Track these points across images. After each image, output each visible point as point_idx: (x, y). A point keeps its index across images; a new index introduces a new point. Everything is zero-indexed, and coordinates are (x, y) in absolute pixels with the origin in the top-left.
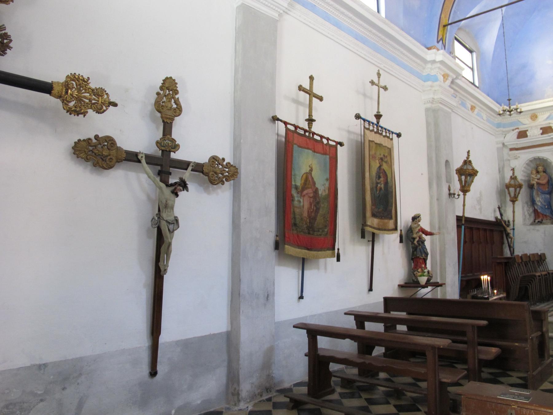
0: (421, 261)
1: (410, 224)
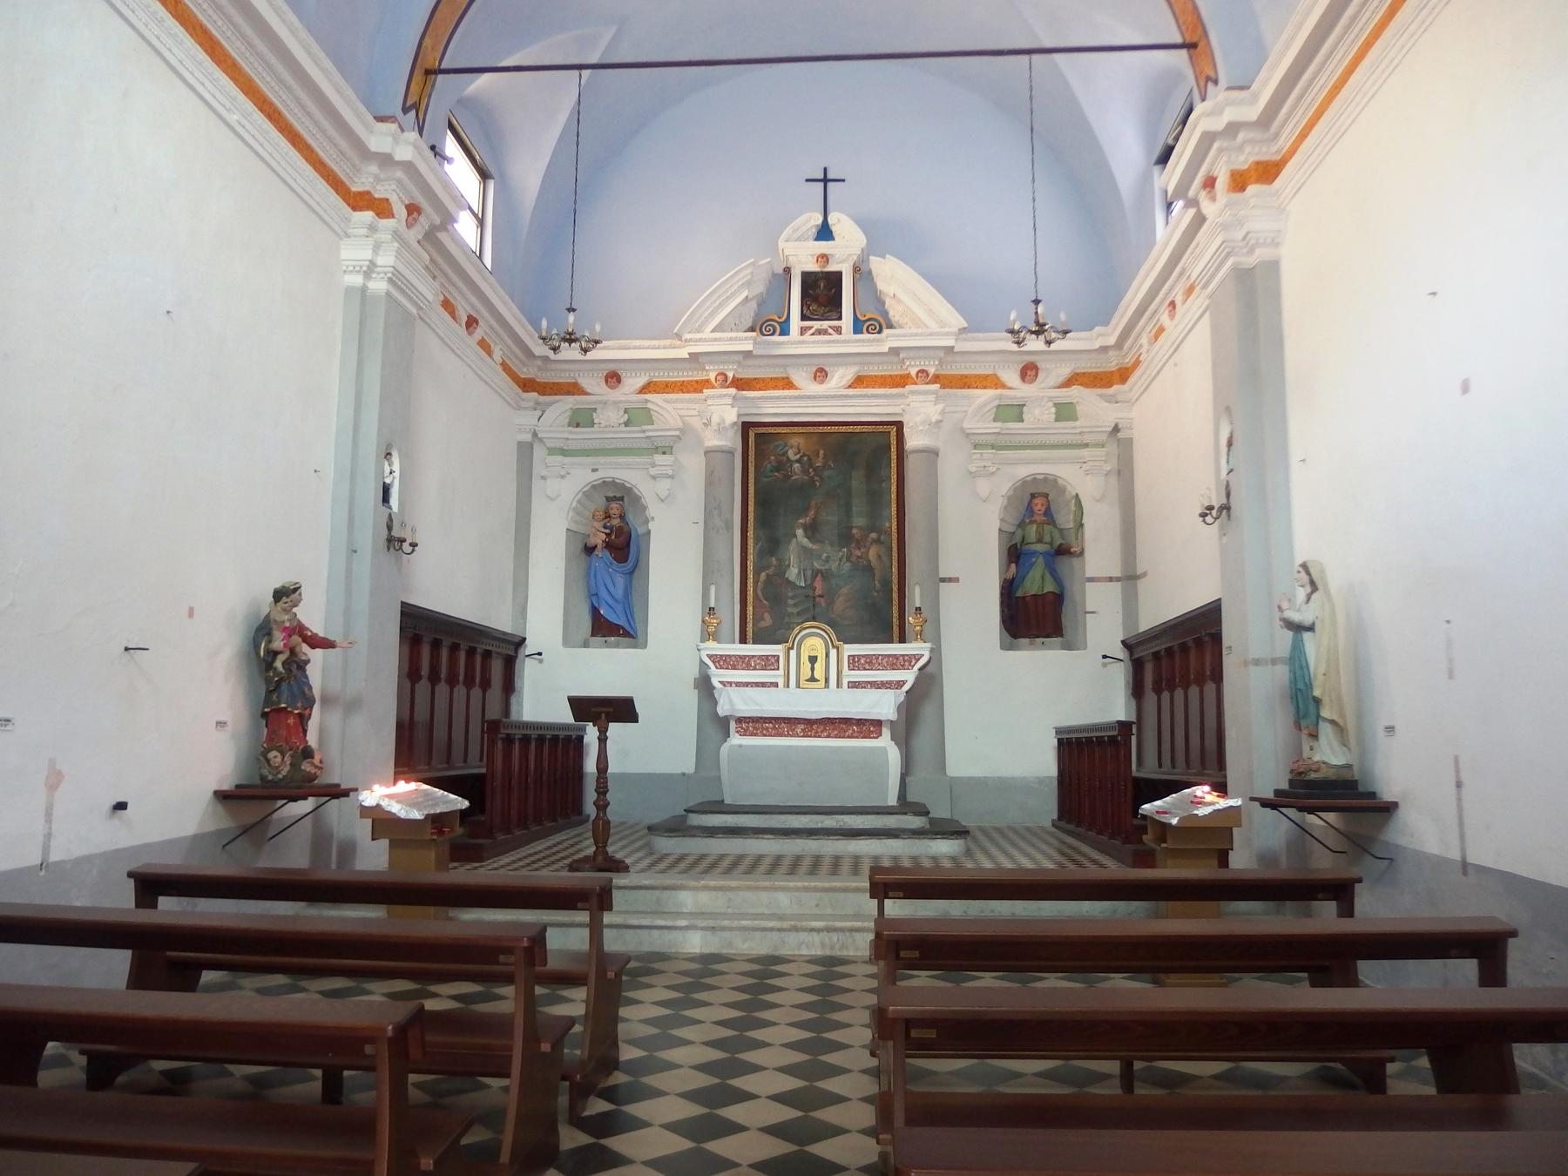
1: (265, 610)
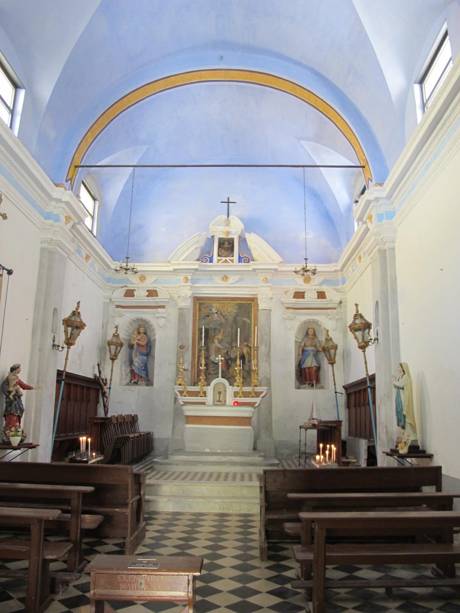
1: (7, 375)
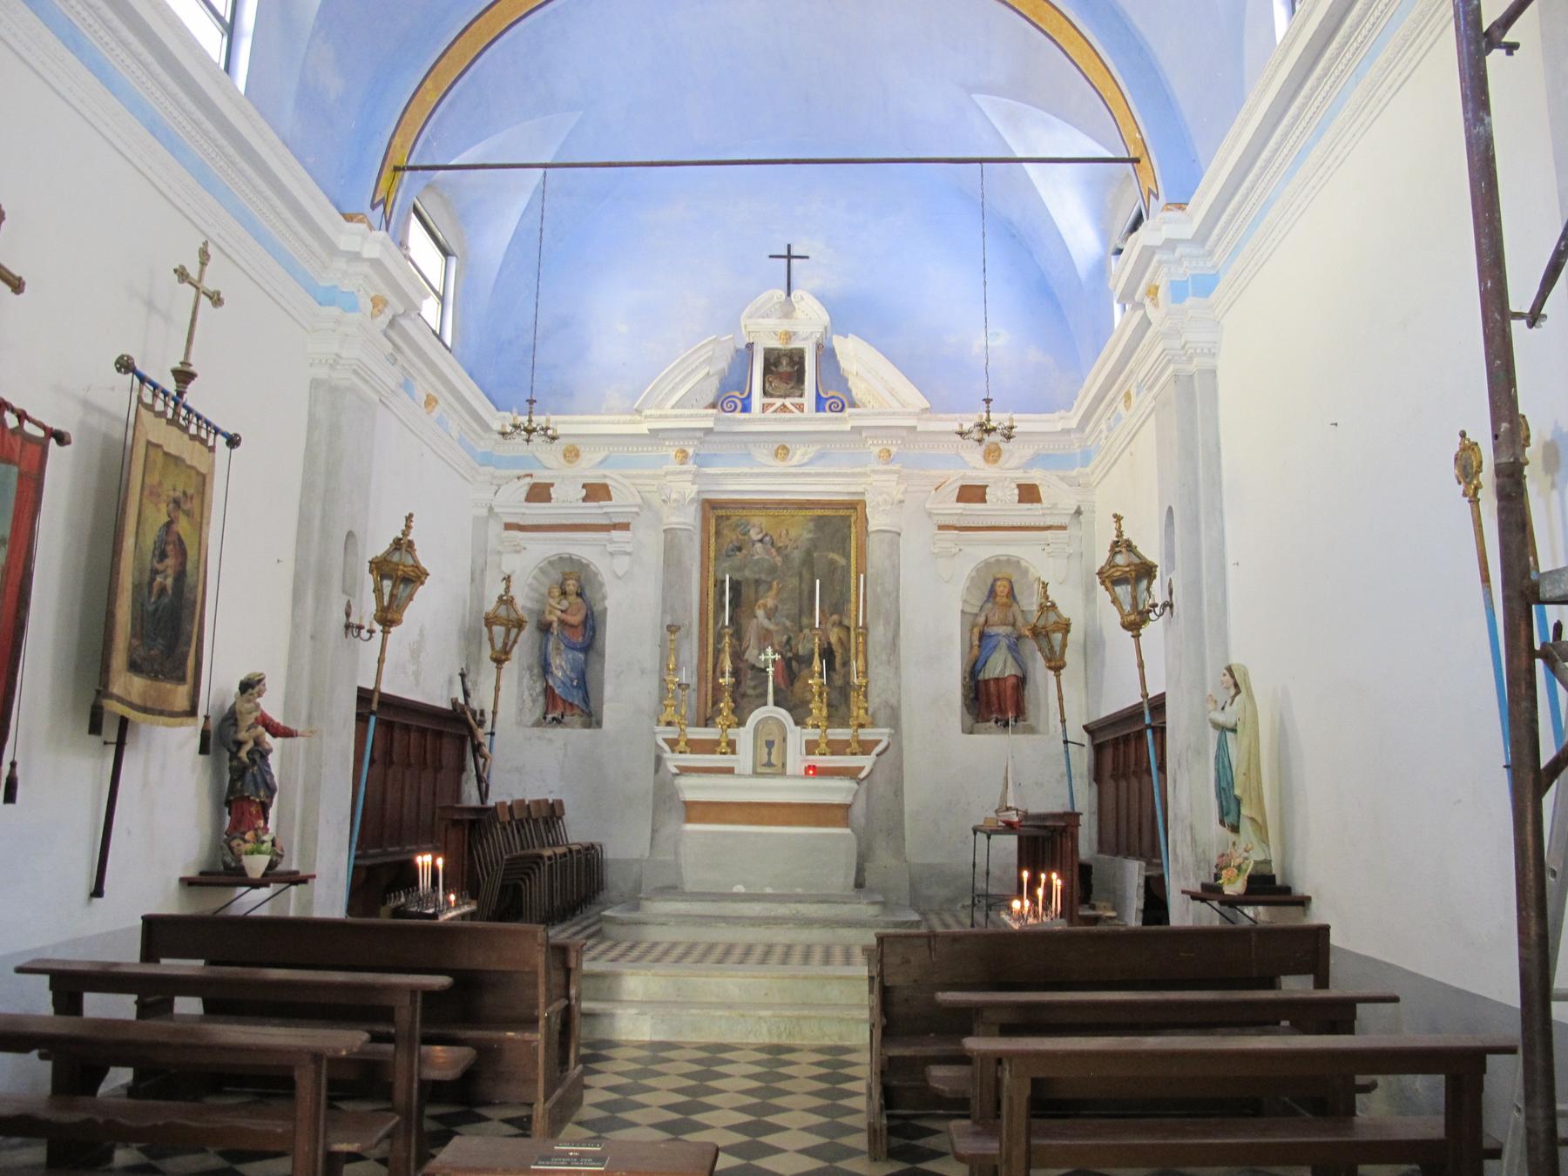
0: (253, 810)
